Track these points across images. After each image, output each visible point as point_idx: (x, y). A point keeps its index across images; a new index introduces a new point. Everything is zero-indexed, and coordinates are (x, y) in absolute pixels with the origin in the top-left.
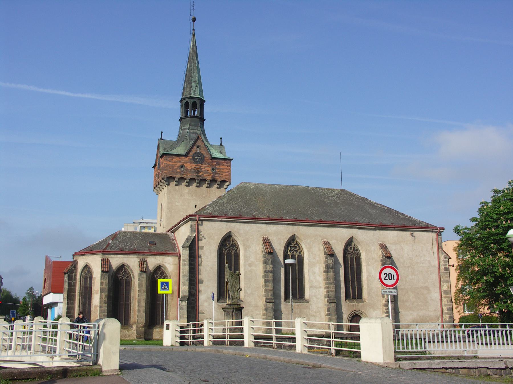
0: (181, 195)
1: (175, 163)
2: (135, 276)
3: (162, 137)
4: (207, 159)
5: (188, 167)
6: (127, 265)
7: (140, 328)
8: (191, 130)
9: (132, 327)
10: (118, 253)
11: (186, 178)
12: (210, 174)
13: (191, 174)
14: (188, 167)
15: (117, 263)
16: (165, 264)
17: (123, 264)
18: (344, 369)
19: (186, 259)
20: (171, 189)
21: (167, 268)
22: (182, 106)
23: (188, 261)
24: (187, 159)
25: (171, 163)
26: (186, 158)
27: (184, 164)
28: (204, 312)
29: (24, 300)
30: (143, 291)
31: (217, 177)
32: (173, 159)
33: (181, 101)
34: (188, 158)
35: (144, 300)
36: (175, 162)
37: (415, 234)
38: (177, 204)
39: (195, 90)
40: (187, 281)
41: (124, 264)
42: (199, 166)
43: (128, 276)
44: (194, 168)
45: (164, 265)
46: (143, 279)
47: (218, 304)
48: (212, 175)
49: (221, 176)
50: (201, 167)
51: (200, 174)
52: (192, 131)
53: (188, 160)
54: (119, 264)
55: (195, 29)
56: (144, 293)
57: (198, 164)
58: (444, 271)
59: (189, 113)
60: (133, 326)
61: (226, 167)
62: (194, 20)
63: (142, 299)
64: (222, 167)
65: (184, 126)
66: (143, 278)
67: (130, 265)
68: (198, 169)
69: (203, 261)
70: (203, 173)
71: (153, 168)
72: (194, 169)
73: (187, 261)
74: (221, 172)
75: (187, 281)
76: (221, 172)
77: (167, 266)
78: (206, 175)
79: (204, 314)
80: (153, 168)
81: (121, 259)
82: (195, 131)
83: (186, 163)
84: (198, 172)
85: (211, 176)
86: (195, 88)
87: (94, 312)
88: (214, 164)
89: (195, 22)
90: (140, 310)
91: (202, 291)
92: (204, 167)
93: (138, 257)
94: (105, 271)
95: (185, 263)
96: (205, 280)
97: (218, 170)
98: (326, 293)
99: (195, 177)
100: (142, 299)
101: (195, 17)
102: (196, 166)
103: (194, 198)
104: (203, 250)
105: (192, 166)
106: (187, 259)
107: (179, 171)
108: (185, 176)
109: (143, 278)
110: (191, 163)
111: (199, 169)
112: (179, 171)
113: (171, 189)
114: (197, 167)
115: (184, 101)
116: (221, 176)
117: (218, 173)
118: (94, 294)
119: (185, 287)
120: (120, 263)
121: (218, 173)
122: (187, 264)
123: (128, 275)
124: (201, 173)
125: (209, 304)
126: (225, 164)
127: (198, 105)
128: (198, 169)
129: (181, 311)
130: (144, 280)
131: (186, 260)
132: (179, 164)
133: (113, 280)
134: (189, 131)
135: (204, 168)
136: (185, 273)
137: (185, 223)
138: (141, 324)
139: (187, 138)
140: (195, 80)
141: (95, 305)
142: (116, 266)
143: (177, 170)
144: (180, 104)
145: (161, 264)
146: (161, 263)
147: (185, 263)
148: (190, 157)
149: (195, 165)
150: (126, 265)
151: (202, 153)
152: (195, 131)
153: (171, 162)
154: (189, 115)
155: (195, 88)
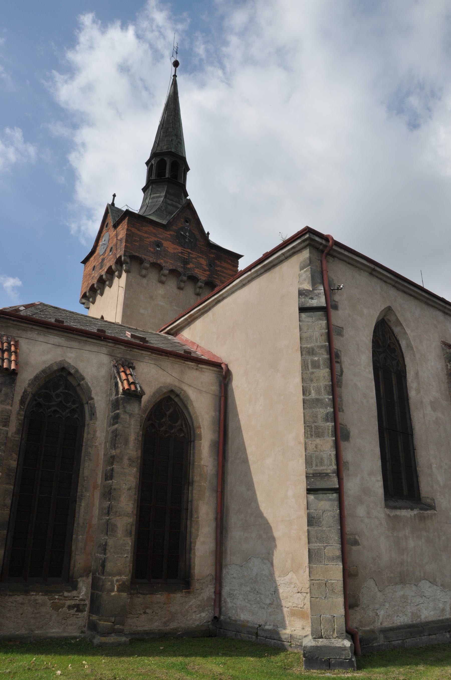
0: (151, 297)
1: (146, 235)
2: (97, 411)
3: (115, 202)
4: (200, 245)
5: (168, 248)
6: (77, 371)
7: (113, 594)
8: (168, 200)
9: (75, 587)
11: (164, 266)
12: (205, 271)
13: (172, 262)
14: (168, 248)
15: (44, 358)
16: (185, 388)
18: (398, 641)
19: (318, 346)
20: (133, 280)
21: (191, 401)
24: (168, 234)
25: (139, 233)
26: (166, 232)
27: (163, 242)
28: (357, 537)
30: (129, 459)
31: (216, 278)
32: (144, 227)
34: (169, 233)
35: (129, 489)
36: (146, 232)
38: (142, 311)
39: (177, 146)
41: (66, 365)
42: (187, 253)
43: (73, 409)
44: (179, 252)
45: (183, 390)
46: (130, 418)
47: (388, 511)
48: (208, 273)
49: (223, 279)
50: (191, 255)
51: (189, 266)
52: (170, 202)
53: (169, 236)
54: (51, 365)
56: (130, 465)
57: (185, 248)
60: (81, 584)
61: (230, 267)
63: (124, 486)
64: (225, 265)
65: (154, 194)
66: (131, 415)
67: (85, 375)
68: (185, 257)
69: (344, 370)
70: (194, 266)
71: (81, 263)
72: (179, 255)
73: (323, 354)
74: (223, 272)
76: (223, 272)
77: (192, 394)
78: (199, 272)
79: (359, 545)
80: (81, 263)
81: (59, 351)
82: (174, 203)
83: (166, 240)
84: (185, 262)
85: (206, 275)
86: (177, 144)
88: (212, 256)
90: (116, 526)
91: (351, 468)
92: (196, 256)
93: (110, 355)
94: (6, 369)
95: (316, 358)
96: (354, 431)
97: (218, 269)
99: (180, 270)
100: (124, 486)
102: (182, 250)
103: (175, 308)
104: (342, 339)
105: (175, 249)
106: (322, 347)
107: (152, 250)
108: (162, 261)
109: (131, 415)
110: (173, 243)
111: (187, 257)
112: (152, 250)
113: (133, 280)
114: (185, 253)
116: (223, 279)
117: (218, 272)
119: (318, 441)
120: (51, 362)
121: (218, 272)
122: (321, 363)
123: (74, 406)
124: (191, 266)
125: (368, 513)
126: (229, 261)
128: (185, 257)
129: (312, 533)
130: (133, 422)
131: (317, 350)
132: (153, 239)
133: (23, 413)
134: (164, 200)
135: (196, 258)
136: (318, 391)
137: (263, 271)
138: (115, 579)
139: (162, 210)
140: (177, 133)
142: (42, 367)
143: (149, 248)
145: (175, 386)
146: (177, 383)
148: (173, 233)
149: (180, 249)
150: (72, 371)
151: (194, 232)
152: (174, 203)
153: (139, 230)
155: (177, 144)
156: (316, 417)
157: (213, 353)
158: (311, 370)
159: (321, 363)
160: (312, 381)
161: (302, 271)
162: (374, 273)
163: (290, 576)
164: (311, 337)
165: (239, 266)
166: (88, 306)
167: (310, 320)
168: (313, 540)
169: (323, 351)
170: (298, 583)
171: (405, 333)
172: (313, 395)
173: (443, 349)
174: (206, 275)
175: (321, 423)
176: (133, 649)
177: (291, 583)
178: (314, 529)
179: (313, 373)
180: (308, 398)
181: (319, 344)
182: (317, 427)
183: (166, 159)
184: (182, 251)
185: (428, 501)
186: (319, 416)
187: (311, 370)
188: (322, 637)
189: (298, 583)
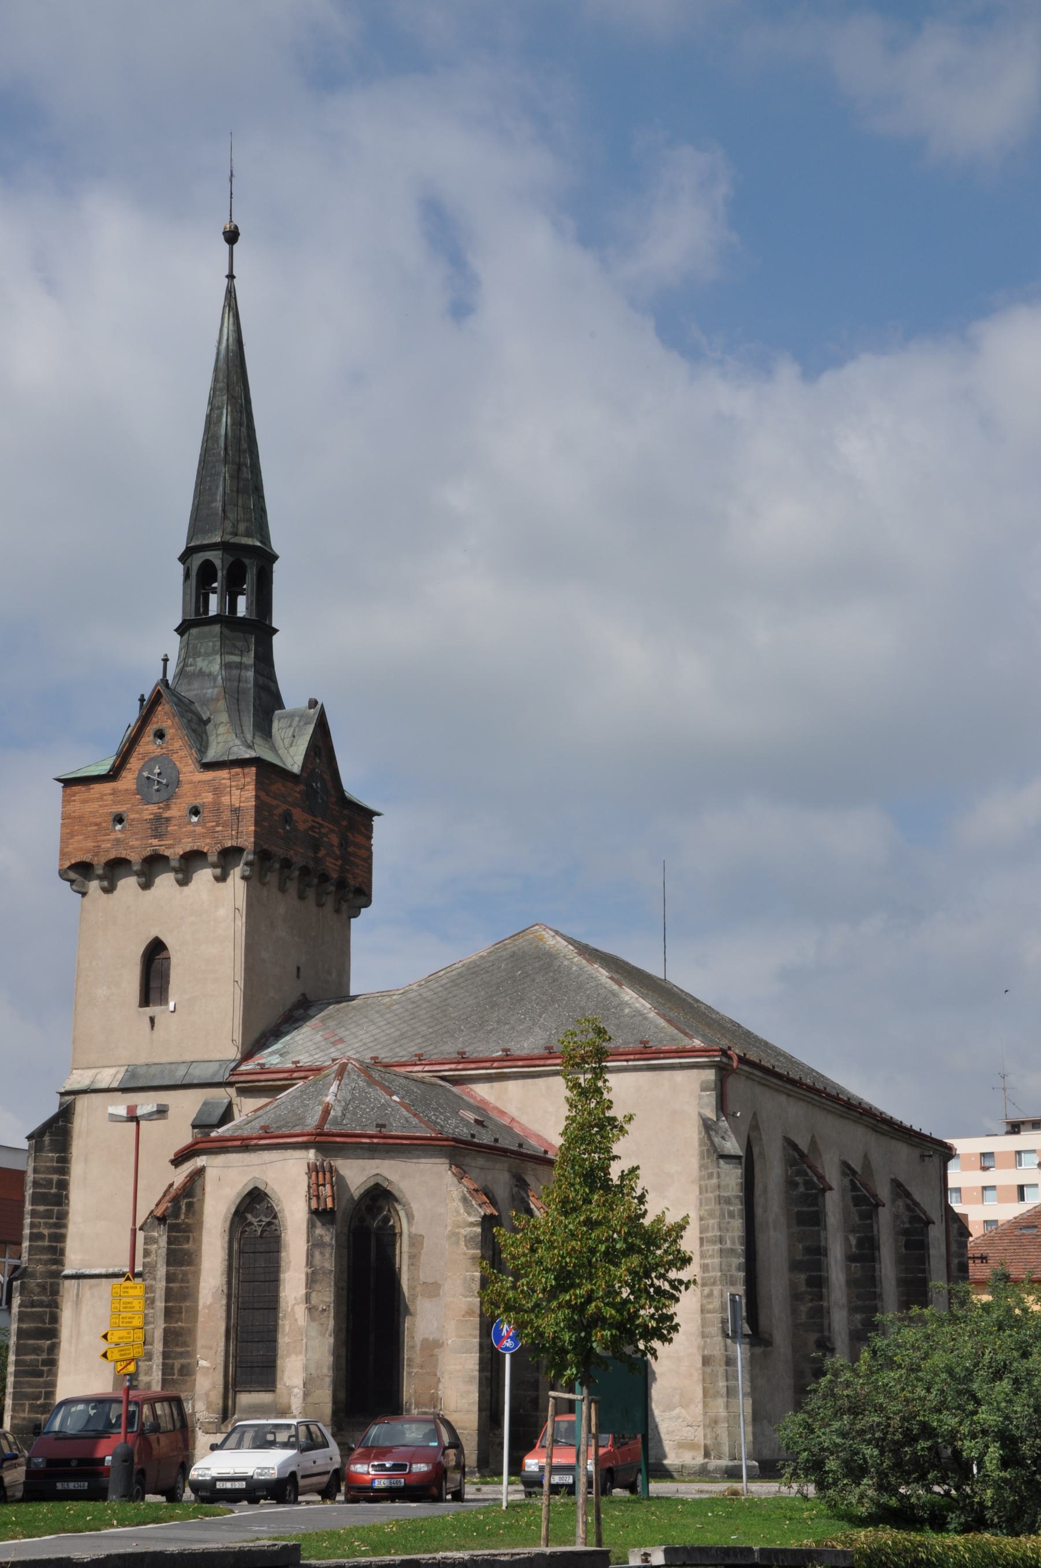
10: (230, 1144)
17: (256, 1188)
22: (187, 576)
23: (739, 1203)
29: (623, 1345)
33: (184, 558)
37: (758, 1061)
40: (739, 1270)
55: (235, 273)
58: (809, 1289)
59: (213, 599)
62: (232, 237)
75: (739, 1270)
85: (337, 868)
87: (422, 1367)
89: (235, 246)
95: (732, 1208)
98: (860, 1326)
101: (236, 227)
106: (737, 1197)
115: (197, 560)
118: (419, 1297)
122: (736, 1213)
127: (251, 576)
136: (733, 1243)
141: (425, 1341)
144: (180, 568)
147: (732, 1208)
154: (213, 609)
156: (731, 1266)
157: (549, 1140)
158: (727, 1220)
159: (736, 1213)
160: (727, 1230)
161: (704, 1093)
162: (750, 1076)
163: (677, 1410)
164: (728, 1186)
165: (373, 835)
166: (84, 890)
167: (727, 1166)
168: (730, 1378)
169: (737, 1201)
170: (688, 1417)
171: (761, 1139)
172: (728, 1245)
173: (784, 1148)
174: (337, 868)
175: (734, 1272)
176: (851, 1442)
177: (680, 1418)
178: (708, 1370)
179: (728, 1223)
180: (724, 1247)
181: (734, 1193)
182: (731, 1276)
183: (246, 561)
184: (314, 824)
185: (766, 1336)
186: (733, 1266)
187: (727, 1220)
188: (735, 1459)
189: (688, 1417)
